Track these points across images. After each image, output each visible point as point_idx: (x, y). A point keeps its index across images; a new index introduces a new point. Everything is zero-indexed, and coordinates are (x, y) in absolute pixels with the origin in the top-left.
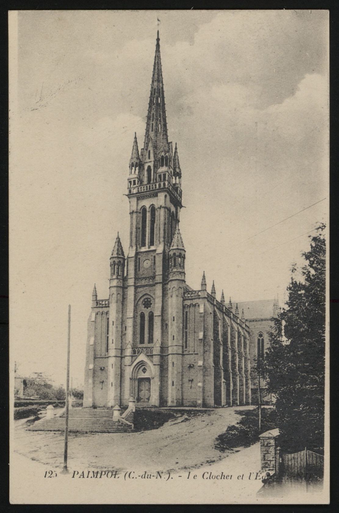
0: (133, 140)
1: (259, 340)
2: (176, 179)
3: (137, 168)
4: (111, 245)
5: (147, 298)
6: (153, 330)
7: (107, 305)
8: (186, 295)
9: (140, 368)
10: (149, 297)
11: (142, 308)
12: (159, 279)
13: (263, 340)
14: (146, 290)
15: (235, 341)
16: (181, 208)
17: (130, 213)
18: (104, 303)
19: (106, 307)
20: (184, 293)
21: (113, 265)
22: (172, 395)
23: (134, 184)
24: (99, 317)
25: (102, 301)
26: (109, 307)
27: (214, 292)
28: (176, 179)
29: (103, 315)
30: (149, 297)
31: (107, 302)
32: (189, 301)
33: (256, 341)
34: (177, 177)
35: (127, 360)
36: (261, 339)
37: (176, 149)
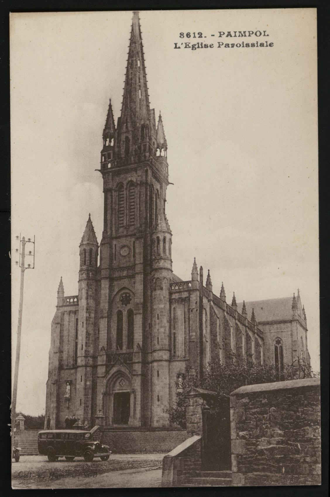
0: (108, 108)
1: (276, 348)
2: (161, 152)
3: (112, 140)
4: (81, 231)
5: (126, 293)
6: (133, 324)
7: (76, 303)
8: (173, 288)
9: (116, 380)
10: (127, 291)
11: (118, 306)
12: (139, 268)
13: (281, 347)
14: (125, 283)
15: (241, 347)
16: (167, 185)
17: (57, 307)
18: (72, 300)
19: (75, 305)
20: (171, 285)
21: (83, 253)
22: (114, 234)
23: (109, 158)
24: (66, 317)
25: (70, 298)
26: (78, 305)
27: (209, 283)
28: (161, 152)
29: (71, 314)
30: (127, 291)
31: (75, 300)
32: (177, 294)
33: (273, 348)
34: (163, 150)
35: (101, 371)
36: (278, 346)
37: (160, 117)
